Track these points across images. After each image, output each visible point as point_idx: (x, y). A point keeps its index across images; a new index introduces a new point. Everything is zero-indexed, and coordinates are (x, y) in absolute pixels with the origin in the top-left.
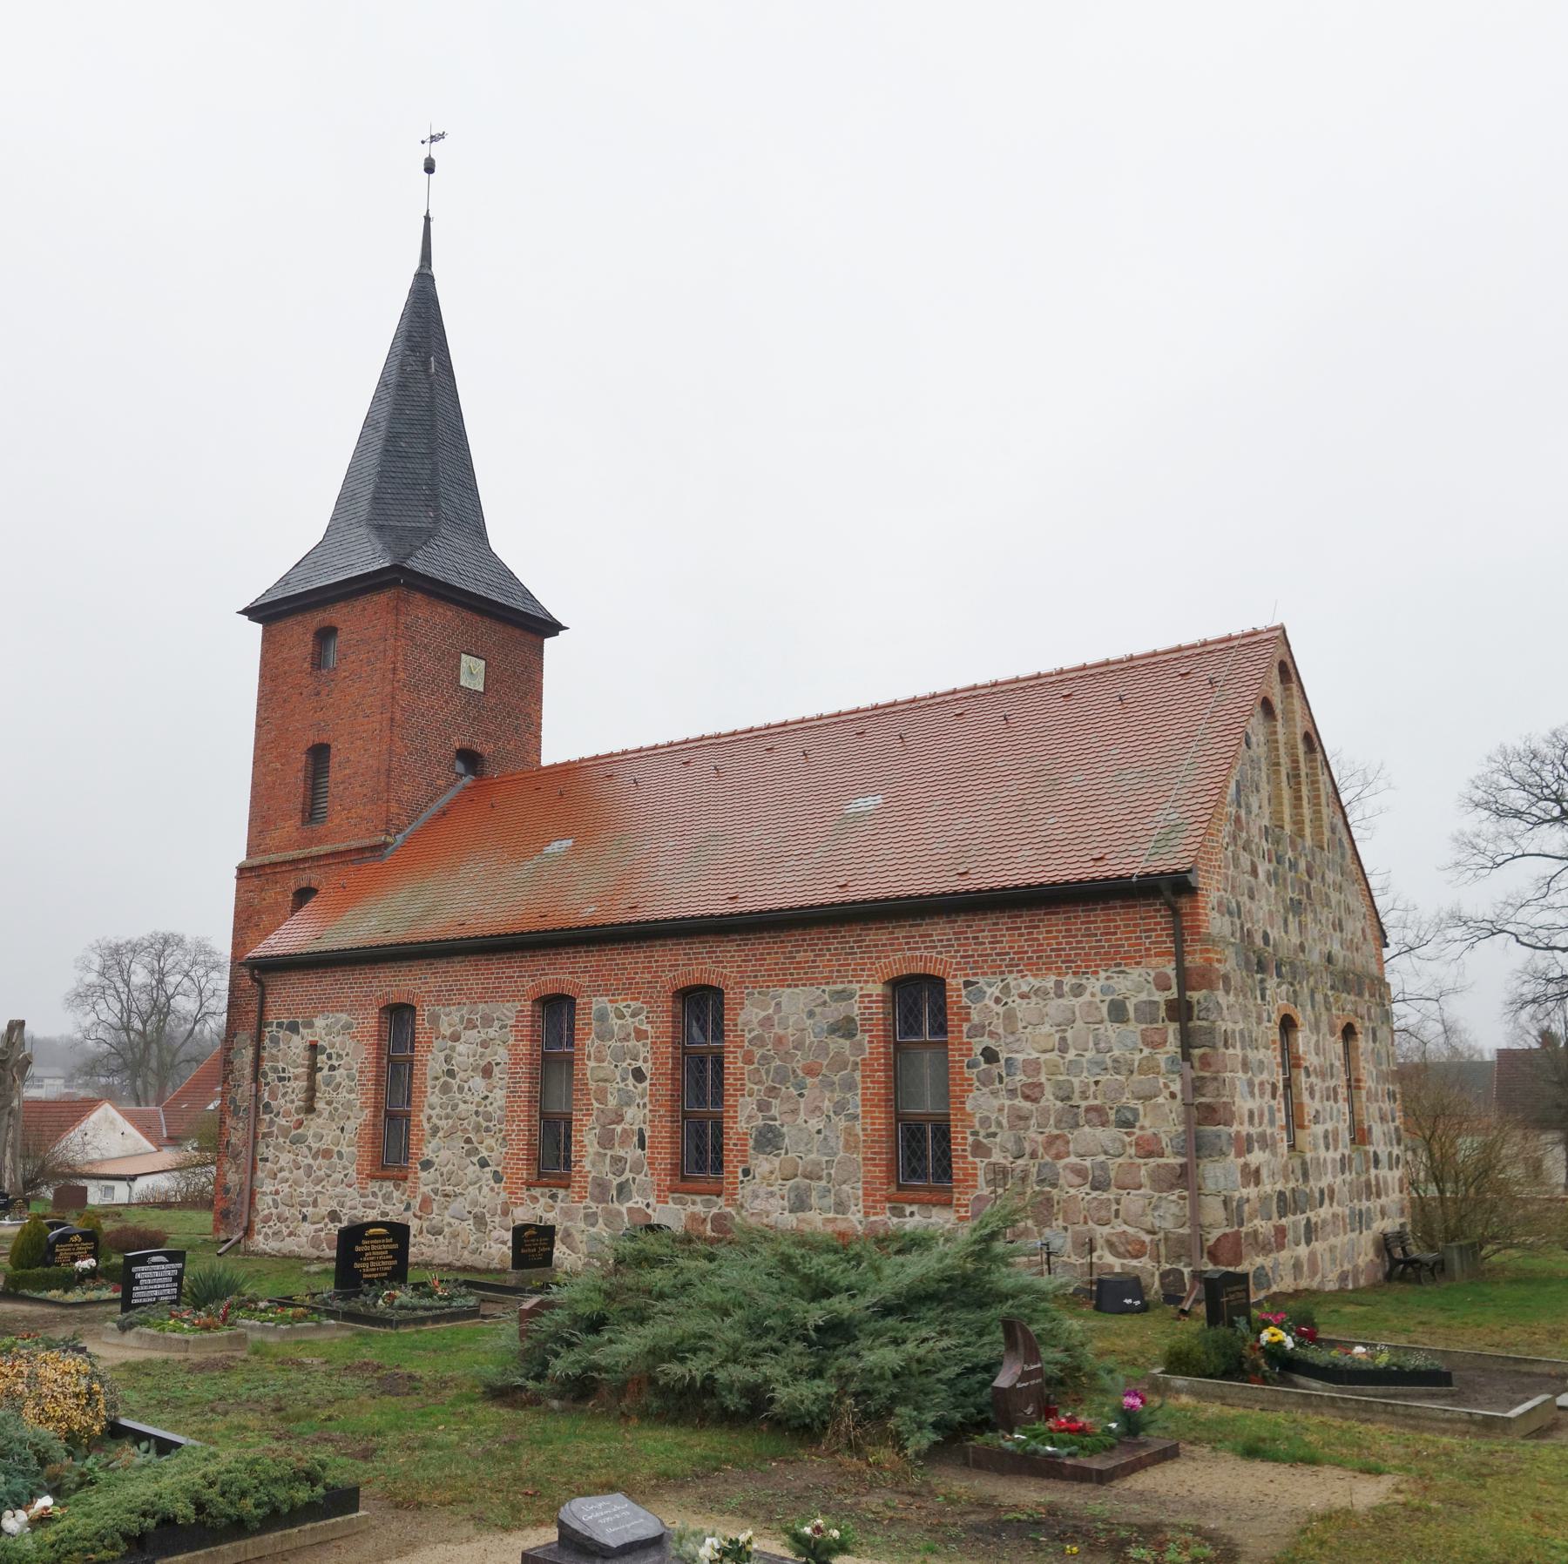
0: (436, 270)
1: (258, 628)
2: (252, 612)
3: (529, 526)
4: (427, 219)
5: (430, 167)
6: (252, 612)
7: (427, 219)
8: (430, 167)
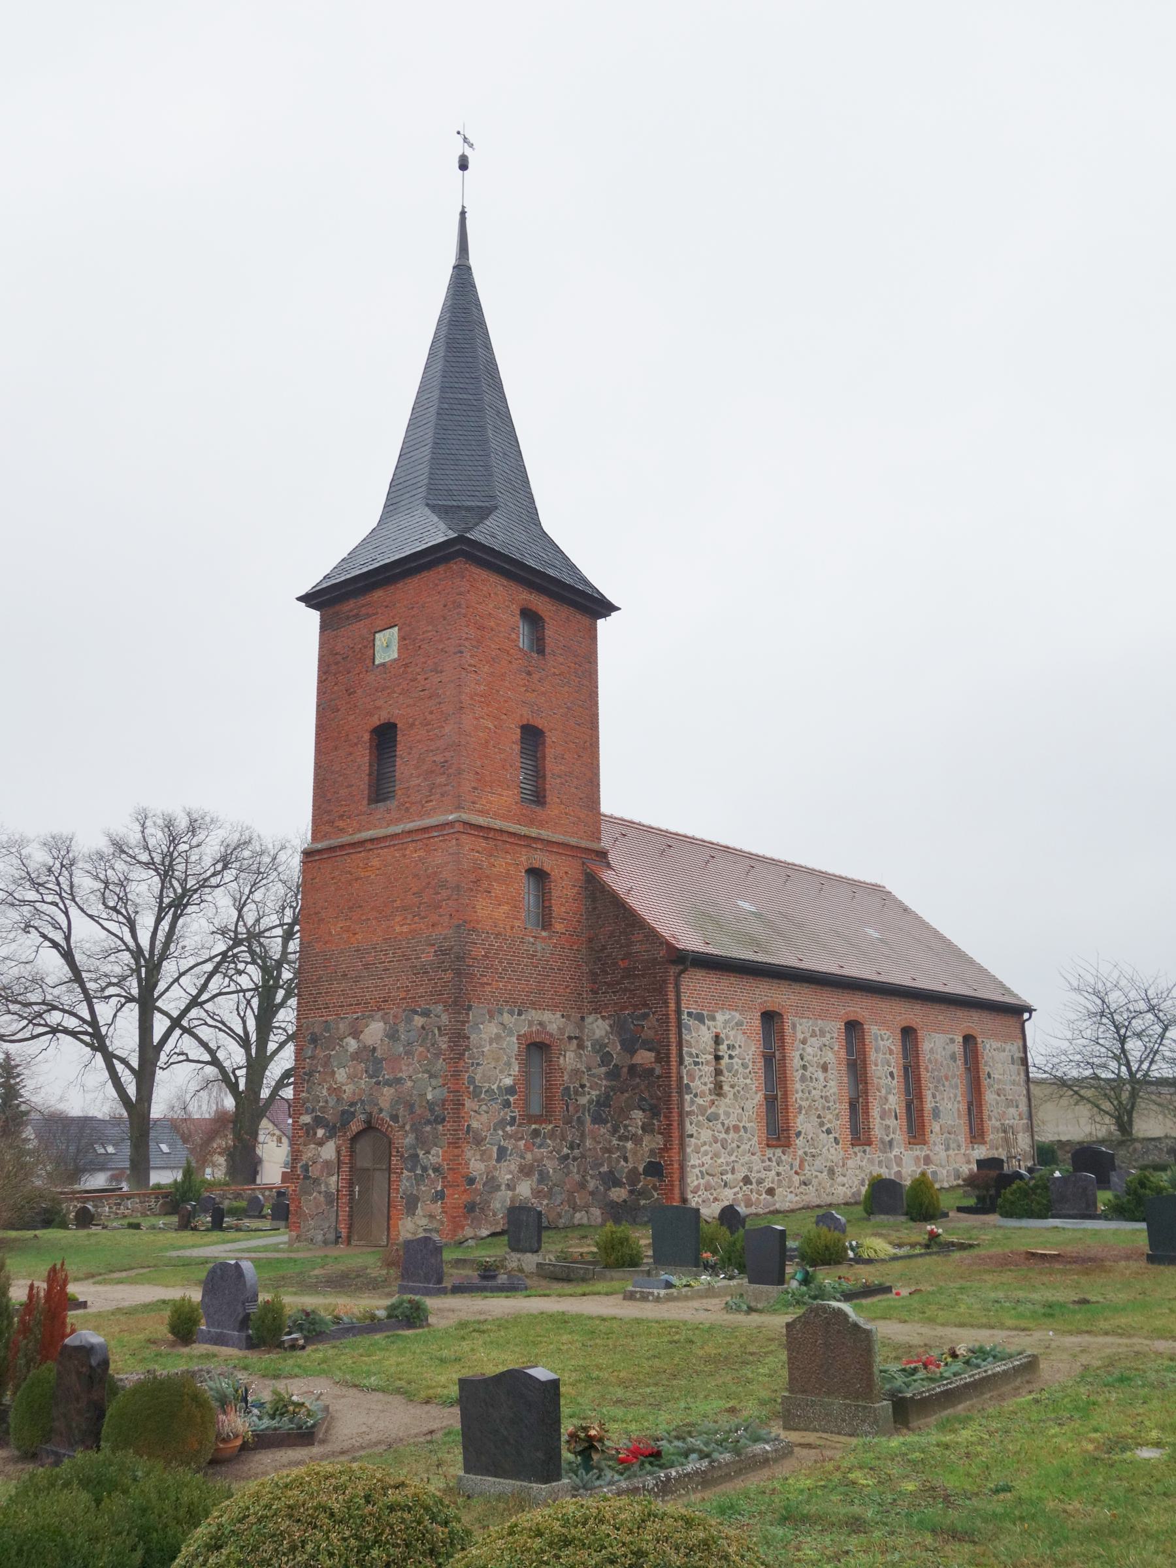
0: (474, 261)
1: (315, 616)
2: (309, 599)
3: (577, 511)
4: (463, 214)
5: (463, 165)
6: (309, 599)
7: (463, 214)
8: (463, 165)
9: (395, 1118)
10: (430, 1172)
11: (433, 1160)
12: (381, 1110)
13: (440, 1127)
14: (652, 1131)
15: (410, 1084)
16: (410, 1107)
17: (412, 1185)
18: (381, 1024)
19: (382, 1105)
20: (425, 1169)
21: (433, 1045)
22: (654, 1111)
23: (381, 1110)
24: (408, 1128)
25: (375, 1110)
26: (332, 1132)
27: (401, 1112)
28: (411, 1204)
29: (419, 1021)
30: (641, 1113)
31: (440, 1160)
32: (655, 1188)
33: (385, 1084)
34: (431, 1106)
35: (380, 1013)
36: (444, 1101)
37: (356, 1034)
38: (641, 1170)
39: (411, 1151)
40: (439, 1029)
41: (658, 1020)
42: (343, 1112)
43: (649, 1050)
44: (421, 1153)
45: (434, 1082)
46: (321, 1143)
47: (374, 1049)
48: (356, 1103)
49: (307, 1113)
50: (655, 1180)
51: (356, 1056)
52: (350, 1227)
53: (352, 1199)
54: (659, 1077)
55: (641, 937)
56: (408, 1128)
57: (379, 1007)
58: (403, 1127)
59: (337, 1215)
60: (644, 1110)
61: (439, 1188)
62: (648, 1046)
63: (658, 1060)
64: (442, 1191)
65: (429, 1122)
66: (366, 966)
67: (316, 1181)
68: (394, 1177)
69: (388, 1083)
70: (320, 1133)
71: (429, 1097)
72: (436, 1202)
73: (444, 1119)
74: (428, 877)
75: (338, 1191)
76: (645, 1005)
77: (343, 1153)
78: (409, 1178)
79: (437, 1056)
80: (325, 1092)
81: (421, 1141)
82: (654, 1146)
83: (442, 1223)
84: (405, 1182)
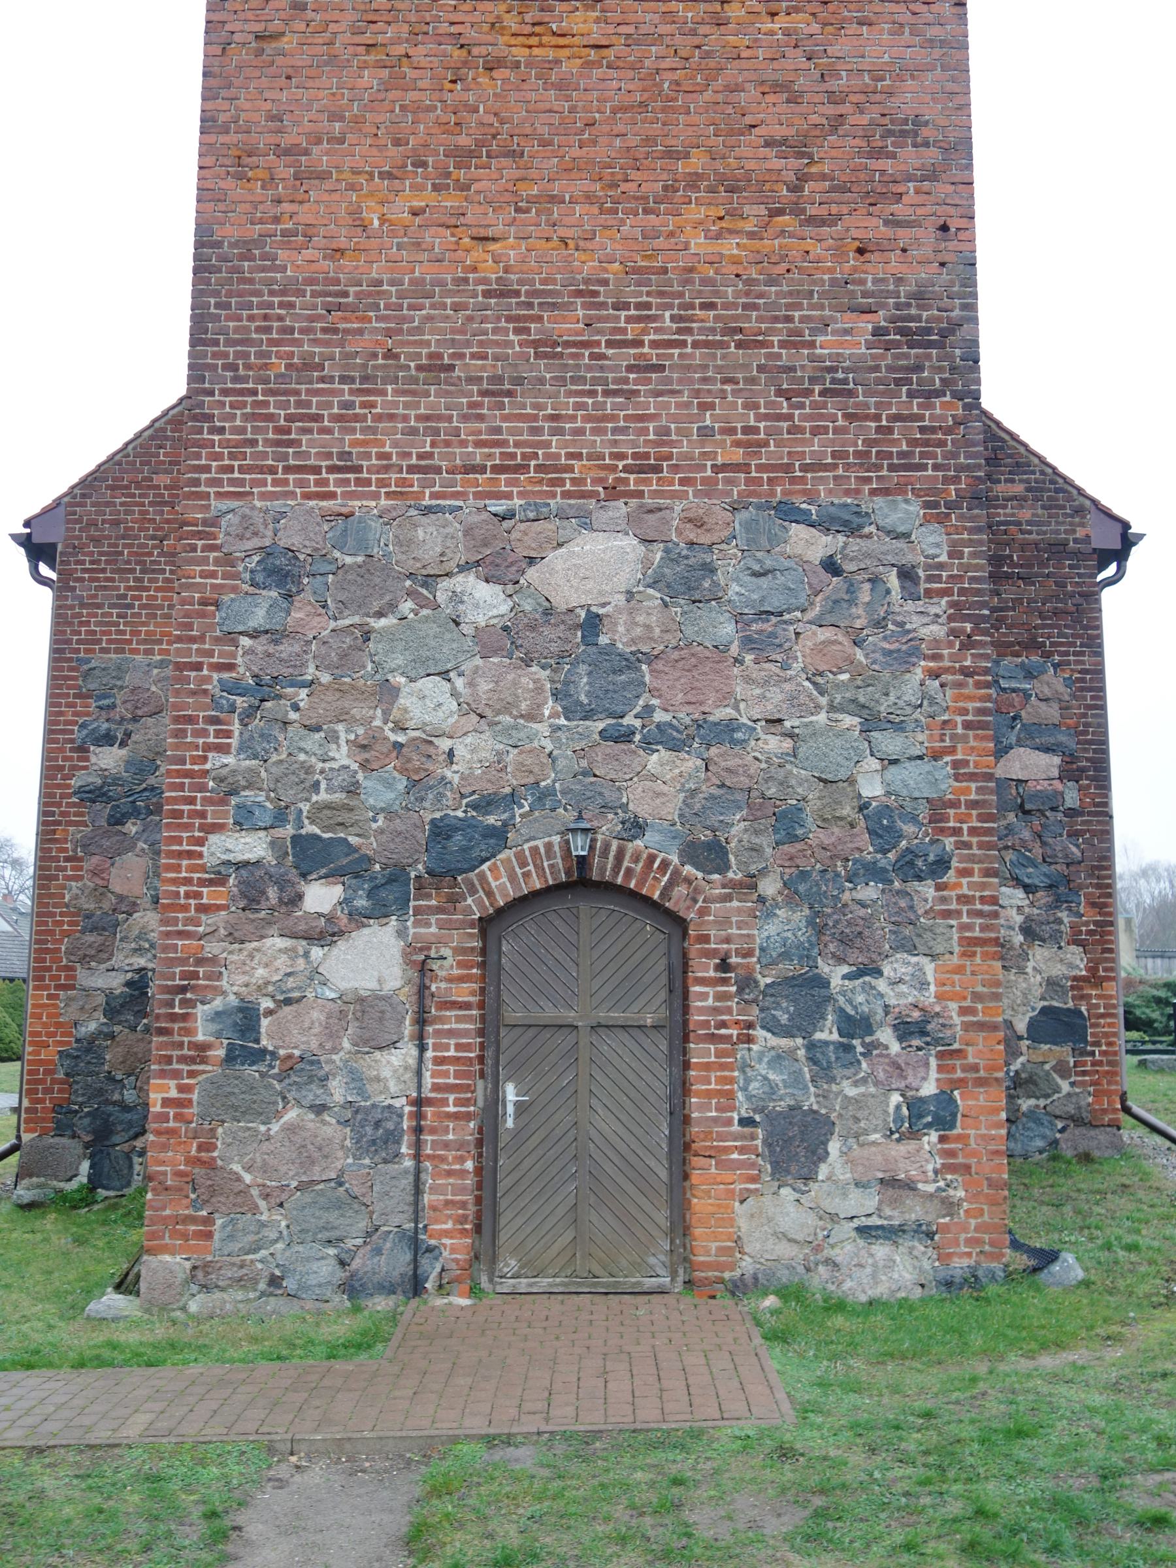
9: (711, 854)
10: (886, 1035)
11: (901, 998)
12: (637, 827)
13: (928, 890)
14: (1055, 937)
15: (774, 744)
16: (788, 825)
17: (796, 1080)
18: (629, 544)
19: (641, 808)
20: (856, 1026)
21: (880, 624)
22: (1060, 890)
23: (637, 827)
24: (770, 887)
25: (608, 827)
26: (383, 891)
27: (737, 831)
28: (795, 1144)
29: (809, 544)
30: (1020, 893)
31: (929, 998)
32: (1062, 1069)
33: (648, 744)
34: (881, 823)
35: (620, 509)
36: (938, 809)
37: (499, 567)
38: (1021, 1026)
39: (788, 968)
40: (907, 574)
41: (1068, 682)
42: (441, 831)
43: (1047, 750)
44: (836, 975)
45: (891, 744)
46: (326, 933)
47: (593, 623)
48: (513, 798)
49: (244, 821)
50: (1064, 1052)
51: (506, 640)
52: (484, 1222)
53: (487, 1138)
54: (1071, 813)
55: (1018, 489)
56: (770, 887)
57: (627, 482)
58: (750, 883)
59: (418, 1190)
60: (1028, 889)
61: (929, 1089)
62: (1037, 737)
63: (1069, 773)
64: (944, 1099)
65: (873, 872)
66: (546, 348)
67: (303, 1070)
68: (701, 1053)
69: (668, 739)
70: (321, 897)
71: (871, 788)
72: (914, 1134)
73: (942, 864)
74: (834, 98)
75: (419, 1102)
76: (1031, 645)
77: (447, 965)
78: (778, 1059)
79: (904, 658)
80: (342, 755)
81: (835, 931)
82: (1058, 970)
83: (950, 1207)
84: (762, 1068)
